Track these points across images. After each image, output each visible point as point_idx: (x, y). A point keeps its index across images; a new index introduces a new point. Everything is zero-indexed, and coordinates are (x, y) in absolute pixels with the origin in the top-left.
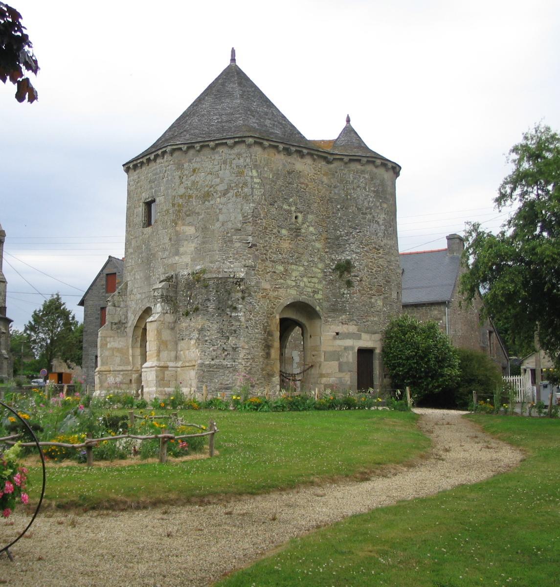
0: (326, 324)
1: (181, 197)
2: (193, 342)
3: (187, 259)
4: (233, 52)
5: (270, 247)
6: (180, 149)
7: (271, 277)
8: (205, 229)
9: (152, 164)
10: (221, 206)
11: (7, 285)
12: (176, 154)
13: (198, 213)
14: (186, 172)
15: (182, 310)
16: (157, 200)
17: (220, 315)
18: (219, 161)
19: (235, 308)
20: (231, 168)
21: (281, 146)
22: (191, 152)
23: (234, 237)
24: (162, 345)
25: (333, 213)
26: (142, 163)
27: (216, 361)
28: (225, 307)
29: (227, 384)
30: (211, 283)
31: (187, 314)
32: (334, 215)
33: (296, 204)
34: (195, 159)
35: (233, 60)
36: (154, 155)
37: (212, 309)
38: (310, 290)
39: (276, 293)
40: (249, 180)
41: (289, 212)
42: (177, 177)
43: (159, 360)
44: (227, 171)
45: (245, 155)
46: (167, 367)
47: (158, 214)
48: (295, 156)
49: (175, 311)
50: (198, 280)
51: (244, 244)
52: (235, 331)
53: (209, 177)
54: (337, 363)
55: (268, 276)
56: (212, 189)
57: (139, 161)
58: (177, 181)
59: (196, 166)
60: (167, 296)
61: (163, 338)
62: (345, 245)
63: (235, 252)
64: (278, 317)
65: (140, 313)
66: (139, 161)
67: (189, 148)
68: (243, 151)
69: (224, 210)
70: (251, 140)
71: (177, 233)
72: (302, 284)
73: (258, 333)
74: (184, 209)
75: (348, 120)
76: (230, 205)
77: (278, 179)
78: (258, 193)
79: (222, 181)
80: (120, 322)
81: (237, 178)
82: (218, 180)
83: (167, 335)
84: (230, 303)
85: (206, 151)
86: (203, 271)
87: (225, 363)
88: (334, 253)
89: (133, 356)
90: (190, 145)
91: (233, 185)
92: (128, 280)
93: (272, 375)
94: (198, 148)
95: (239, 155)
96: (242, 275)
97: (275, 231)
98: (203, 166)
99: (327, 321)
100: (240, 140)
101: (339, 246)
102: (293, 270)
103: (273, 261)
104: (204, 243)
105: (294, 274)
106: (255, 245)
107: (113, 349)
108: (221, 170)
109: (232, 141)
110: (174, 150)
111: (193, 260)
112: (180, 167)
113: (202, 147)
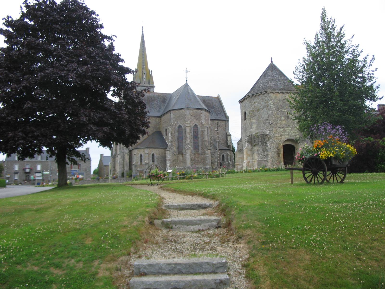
1: (251, 111)
2: (256, 154)
3: (254, 130)
4: (271, 58)
5: (278, 124)
7: (279, 132)
8: (258, 120)
9: (245, 101)
10: (262, 113)
11: (232, 137)
12: (249, 98)
13: (256, 116)
14: (252, 103)
15: (253, 145)
17: (262, 145)
19: (266, 143)
21: (280, 92)
22: (253, 97)
23: (266, 122)
24: (248, 155)
27: (262, 159)
28: (264, 143)
30: (259, 136)
31: (254, 146)
33: (287, 109)
35: (272, 62)
38: (294, 135)
39: (281, 137)
40: (269, 104)
41: (285, 112)
43: (247, 160)
45: (267, 97)
46: (250, 162)
48: (286, 93)
49: (252, 145)
50: (256, 136)
52: (267, 150)
55: (277, 132)
59: (255, 101)
60: (248, 141)
61: (248, 153)
64: (282, 144)
67: (252, 96)
69: (263, 114)
70: (269, 92)
71: (251, 122)
72: (291, 134)
73: (275, 150)
74: (253, 115)
76: (264, 112)
77: (279, 102)
80: (241, 149)
82: (261, 105)
83: (249, 152)
84: (265, 142)
85: (257, 97)
86: (257, 133)
87: (265, 159)
91: (265, 106)
93: (281, 162)
95: (266, 97)
96: (268, 133)
97: (279, 118)
99: (300, 144)
102: (287, 129)
103: (279, 128)
105: (287, 131)
106: (272, 124)
107: (239, 158)
109: (263, 93)
111: (256, 130)
112: (250, 102)
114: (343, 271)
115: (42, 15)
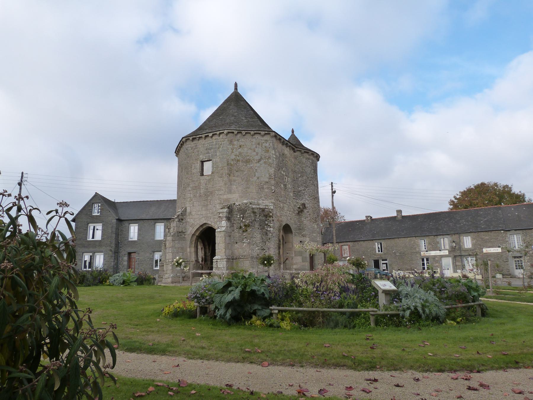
4: (236, 85)
6: (233, 133)
9: (208, 139)
10: (256, 168)
22: (239, 135)
25: (297, 178)
28: (263, 226)
35: (236, 88)
42: (230, 149)
44: (260, 149)
47: (215, 169)
53: (250, 151)
56: (251, 158)
57: (198, 136)
58: (230, 150)
59: (242, 144)
62: (303, 196)
66: (198, 136)
68: (269, 139)
75: (293, 132)
78: (275, 163)
79: (257, 154)
81: (265, 153)
89: (190, 252)
90: (239, 131)
91: (263, 157)
98: (246, 144)
100: (268, 132)
101: (300, 196)
104: (247, 188)
108: (256, 148)
109: (264, 133)
110: (220, 133)
112: (231, 142)
114: (303, 335)
115: (197, 333)
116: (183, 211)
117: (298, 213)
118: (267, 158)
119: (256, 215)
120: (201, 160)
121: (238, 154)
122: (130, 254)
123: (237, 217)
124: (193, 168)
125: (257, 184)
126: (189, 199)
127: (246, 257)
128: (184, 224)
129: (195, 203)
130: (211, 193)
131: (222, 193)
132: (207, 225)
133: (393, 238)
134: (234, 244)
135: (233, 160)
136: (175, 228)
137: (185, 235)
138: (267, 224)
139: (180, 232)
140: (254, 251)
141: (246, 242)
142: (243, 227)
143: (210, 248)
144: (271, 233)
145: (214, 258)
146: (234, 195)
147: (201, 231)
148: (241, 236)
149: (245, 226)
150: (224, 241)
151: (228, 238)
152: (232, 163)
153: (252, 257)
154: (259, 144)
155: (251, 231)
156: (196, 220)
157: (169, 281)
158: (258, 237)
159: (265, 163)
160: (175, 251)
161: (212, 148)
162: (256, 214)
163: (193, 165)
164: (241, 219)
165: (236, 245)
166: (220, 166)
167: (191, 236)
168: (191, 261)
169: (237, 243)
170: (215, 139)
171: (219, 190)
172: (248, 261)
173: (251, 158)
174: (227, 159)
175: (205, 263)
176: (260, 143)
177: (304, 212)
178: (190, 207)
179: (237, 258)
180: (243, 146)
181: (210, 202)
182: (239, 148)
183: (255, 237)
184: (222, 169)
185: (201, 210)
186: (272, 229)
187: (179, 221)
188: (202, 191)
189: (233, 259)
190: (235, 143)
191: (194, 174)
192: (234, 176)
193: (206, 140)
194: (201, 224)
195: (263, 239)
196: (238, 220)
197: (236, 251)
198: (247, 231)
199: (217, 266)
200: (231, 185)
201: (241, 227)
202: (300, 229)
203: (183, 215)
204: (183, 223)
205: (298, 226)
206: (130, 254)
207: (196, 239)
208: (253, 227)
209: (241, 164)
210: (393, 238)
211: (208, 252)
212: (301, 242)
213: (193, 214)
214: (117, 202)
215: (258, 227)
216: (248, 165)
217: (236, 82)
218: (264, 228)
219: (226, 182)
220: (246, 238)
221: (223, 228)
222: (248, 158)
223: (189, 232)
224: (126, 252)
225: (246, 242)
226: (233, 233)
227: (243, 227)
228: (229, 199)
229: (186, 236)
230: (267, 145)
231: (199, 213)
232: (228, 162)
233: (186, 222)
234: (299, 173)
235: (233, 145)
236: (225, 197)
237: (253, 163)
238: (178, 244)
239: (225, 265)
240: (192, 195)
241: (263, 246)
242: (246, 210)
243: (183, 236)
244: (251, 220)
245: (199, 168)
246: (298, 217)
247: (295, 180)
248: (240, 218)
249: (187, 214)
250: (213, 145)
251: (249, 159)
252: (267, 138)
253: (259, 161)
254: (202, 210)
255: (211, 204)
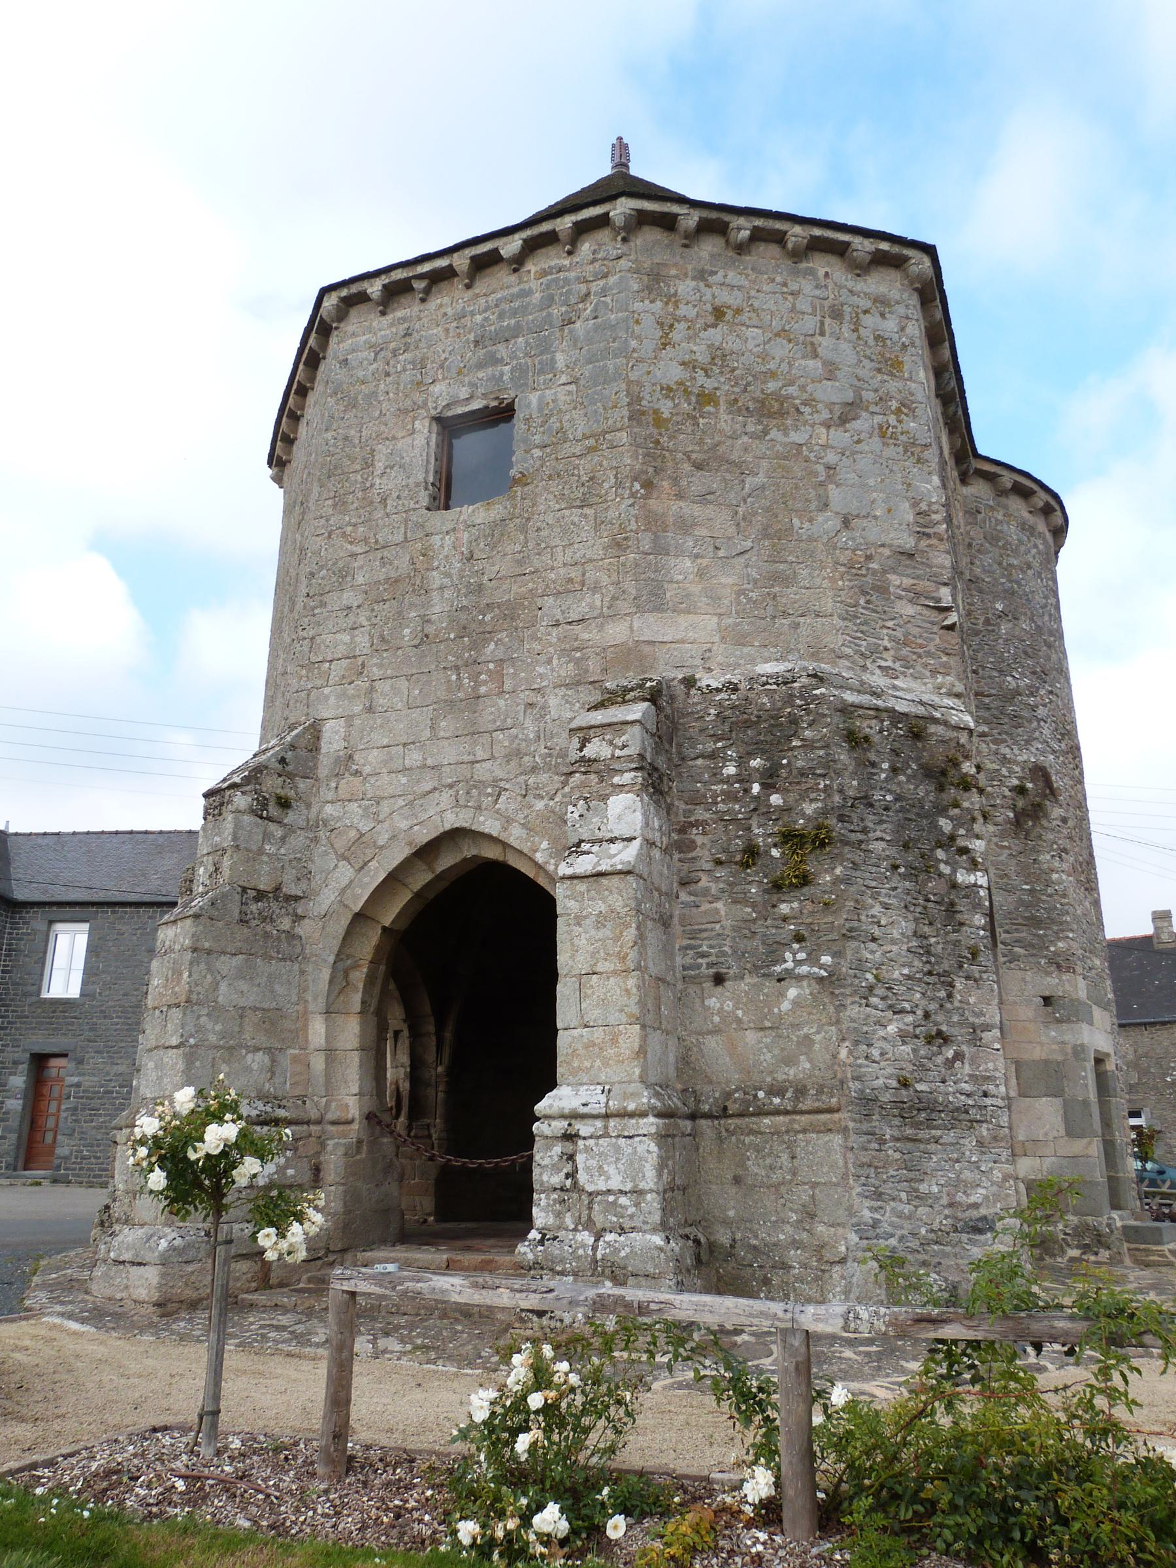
0: (1012, 966)
10: (831, 457)
16: (529, 403)
18: (817, 302)
20: (859, 338)
22: (709, 247)
23: (895, 579)
25: (987, 622)
26: (449, 273)
29: (976, 1206)
32: (990, 628)
34: (721, 273)
36: (525, 241)
37: (883, 844)
42: (648, 321)
47: (537, 453)
51: (926, 612)
53: (780, 349)
54: (1058, 1101)
56: (792, 390)
58: (649, 330)
59: (725, 297)
62: (1030, 722)
63: (899, 634)
65: (399, 854)
79: (831, 371)
81: (879, 377)
85: (767, 253)
88: (1006, 741)
89: (330, 1052)
90: (714, 215)
91: (868, 396)
92: (325, 715)
94: (745, 234)
98: (756, 304)
100: (896, 249)
101: (1017, 720)
104: (775, 578)
113: (758, 236)
116: (292, 747)
117: (1018, 823)
118: (894, 404)
119: (873, 765)
120: (433, 413)
121: (702, 357)
122: (40, 1061)
123: (716, 774)
124: (380, 466)
125: (843, 559)
126: (338, 669)
127: (808, 1103)
128: (298, 840)
129: (384, 687)
130: (509, 613)
131: (592, 607)
132: (469, 850)
133: (1164, 1023)
134: (692, 989)
135: (669, 389)
136: (226, 863)
137: (298, 918)
138: (952, 838)
139: (260, 896)
140: (875, 1053)
141: (804, 969)
142: (775, 853)
143: (448, 1035)
144: (976, 906)
145: (540, 1107)
146: (683, 621)
147: (418, 895)
148: (759, 927)
149: (790, 838)
150: (633, 955)
151: (654, 935)
152: (666, 408)
153: (867, 1103)
154: (836, 314)
155: (847, 880)
156: (385, 807)
157: (142, 1293)
158: (896, 934)
159: (883, 435)
160: (213, 1038)
161: (518, 327)
162: (872, 756)
163: (382, 450)
164: (756, 788)
165: (717, 1001)
166: (581, 428)
167: (345, 921)
168: (330, 1116)
169: (719, 980)
170: (544, 273)
171: (567, 589)
172: (837, 1140)
173: (792, 390)
174: (629, 383)
175: (409, 1128)
176: (847, 309)
177: (1046, 816)
178: (349, 719)
179: (733, 1108)
180: (738, 311)
181: (498, 677)
182: (711, 319)
183: (876, 931)
184: (591, 450)
185: (427, 733)
186: (981, 879)
187: (260, 810)
188: (438, 607)
189: (693, 1117)
190: (685, 288)
191: (384, 501)
192: (680, 496)
193: (480, 287)
194: (424, 835)
195: (928, 953)
196: (730, 797)
197: (712, 1043)
198: (805, 880)
199: (571, 1175)
200: (660, 549)
201: (752, 853)
202: (1035, 922)
203: (291, 776)
204: (291, 829)
205: (1021, 902)
206: (40, 1061)
207: (378, 949)
208: (858, 857)
209: (725, 421)
210: (1164, 1023)
211: (431, 1056)
212: (1047, 1001)
213: (367, 770)
214: (16, 834)
215: (892, 851)
216: (774, 434)
217: (620, 139)
218: (928, 867)
219: (622, 529)
220: (799, 938)
221: (614, 848)
222: (772, 386)
223: (326, 899)
224: (24, 1051)
225: (804, 969)
226: (684, 897)
227: (775, 853)
228: (647, 649)
229: (303, 929)
230: (890, 325)
231: (414, 758)
232: (635, 399)
233: (313, 826)
234: (997, 597)
235: (672, 299)
236: (617, 632)
237: (805, 423)
238: (243, 985)
239: (650, 1172)
240: (362, 641)
241: (933, 1007)
242: (794, 721)
243: (286, 923)
244: (837, 798)
245: (420, 461)
246: (1015, 844)
247: (977, 633)
248: (744, 779)
249: (324, 767)
250: (524, 309)
251: (781, 399)
252: (882, 289)
253: (845, 415)
254: (435, 737)
255: (507, 686)
